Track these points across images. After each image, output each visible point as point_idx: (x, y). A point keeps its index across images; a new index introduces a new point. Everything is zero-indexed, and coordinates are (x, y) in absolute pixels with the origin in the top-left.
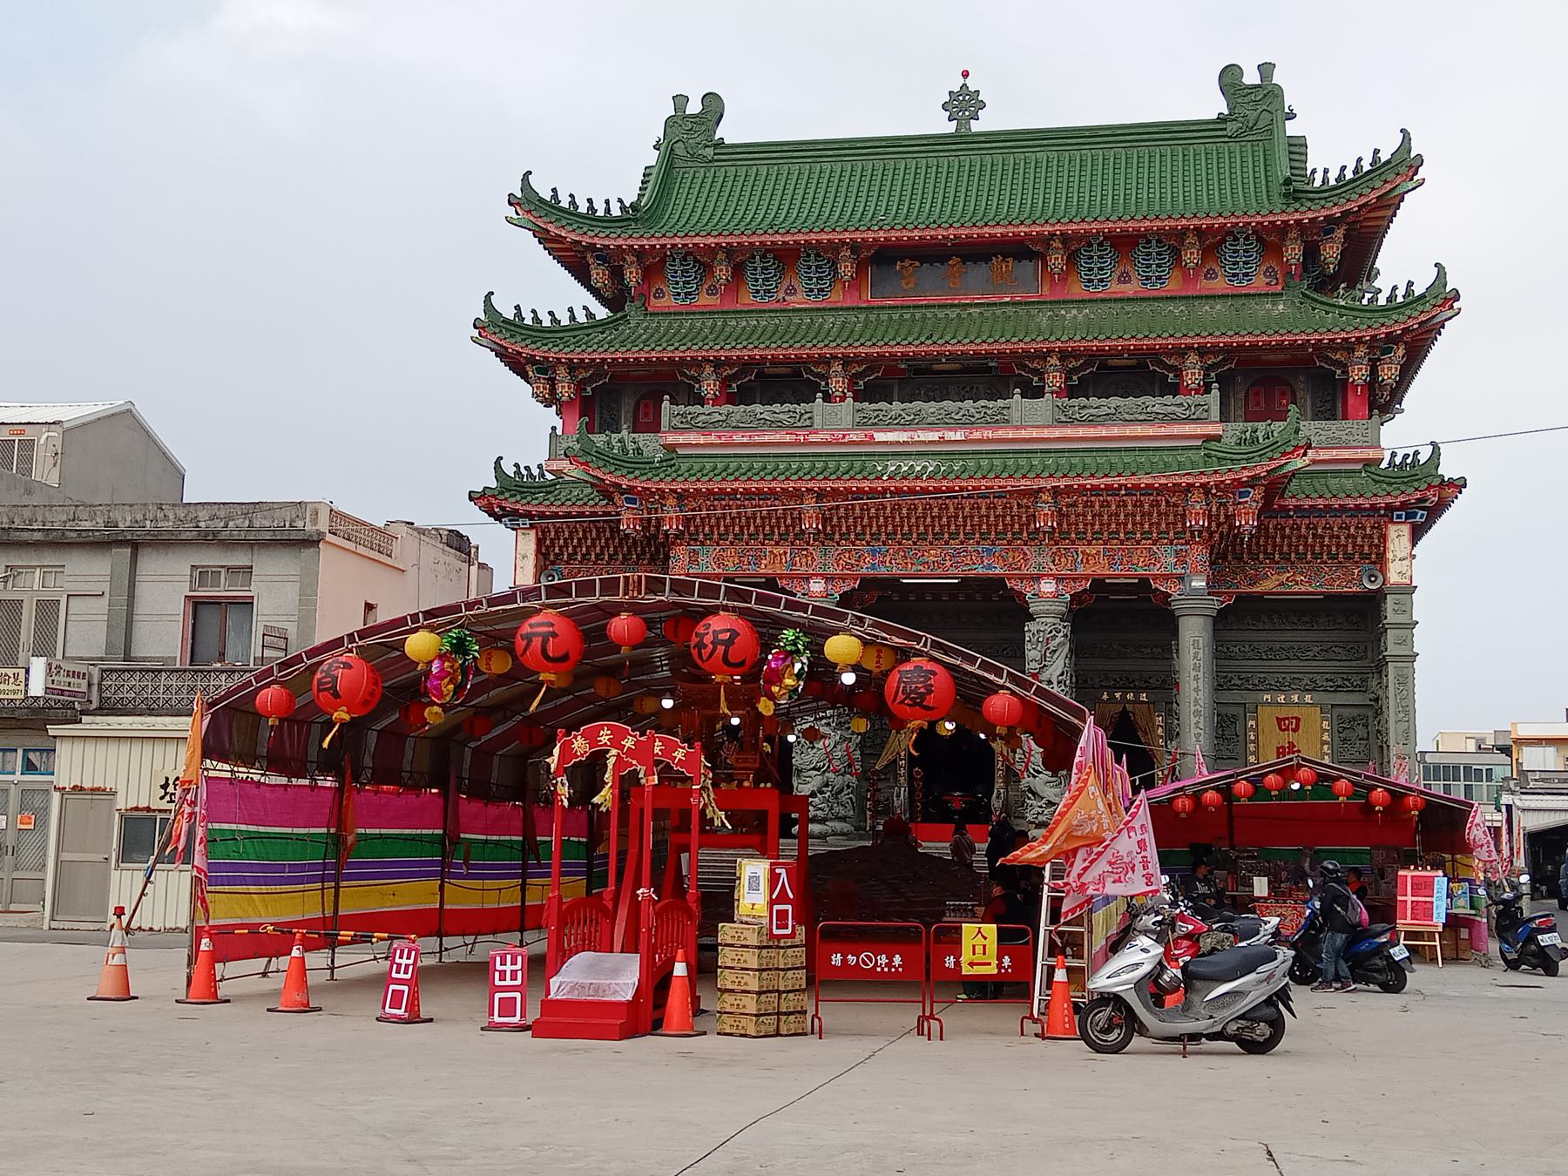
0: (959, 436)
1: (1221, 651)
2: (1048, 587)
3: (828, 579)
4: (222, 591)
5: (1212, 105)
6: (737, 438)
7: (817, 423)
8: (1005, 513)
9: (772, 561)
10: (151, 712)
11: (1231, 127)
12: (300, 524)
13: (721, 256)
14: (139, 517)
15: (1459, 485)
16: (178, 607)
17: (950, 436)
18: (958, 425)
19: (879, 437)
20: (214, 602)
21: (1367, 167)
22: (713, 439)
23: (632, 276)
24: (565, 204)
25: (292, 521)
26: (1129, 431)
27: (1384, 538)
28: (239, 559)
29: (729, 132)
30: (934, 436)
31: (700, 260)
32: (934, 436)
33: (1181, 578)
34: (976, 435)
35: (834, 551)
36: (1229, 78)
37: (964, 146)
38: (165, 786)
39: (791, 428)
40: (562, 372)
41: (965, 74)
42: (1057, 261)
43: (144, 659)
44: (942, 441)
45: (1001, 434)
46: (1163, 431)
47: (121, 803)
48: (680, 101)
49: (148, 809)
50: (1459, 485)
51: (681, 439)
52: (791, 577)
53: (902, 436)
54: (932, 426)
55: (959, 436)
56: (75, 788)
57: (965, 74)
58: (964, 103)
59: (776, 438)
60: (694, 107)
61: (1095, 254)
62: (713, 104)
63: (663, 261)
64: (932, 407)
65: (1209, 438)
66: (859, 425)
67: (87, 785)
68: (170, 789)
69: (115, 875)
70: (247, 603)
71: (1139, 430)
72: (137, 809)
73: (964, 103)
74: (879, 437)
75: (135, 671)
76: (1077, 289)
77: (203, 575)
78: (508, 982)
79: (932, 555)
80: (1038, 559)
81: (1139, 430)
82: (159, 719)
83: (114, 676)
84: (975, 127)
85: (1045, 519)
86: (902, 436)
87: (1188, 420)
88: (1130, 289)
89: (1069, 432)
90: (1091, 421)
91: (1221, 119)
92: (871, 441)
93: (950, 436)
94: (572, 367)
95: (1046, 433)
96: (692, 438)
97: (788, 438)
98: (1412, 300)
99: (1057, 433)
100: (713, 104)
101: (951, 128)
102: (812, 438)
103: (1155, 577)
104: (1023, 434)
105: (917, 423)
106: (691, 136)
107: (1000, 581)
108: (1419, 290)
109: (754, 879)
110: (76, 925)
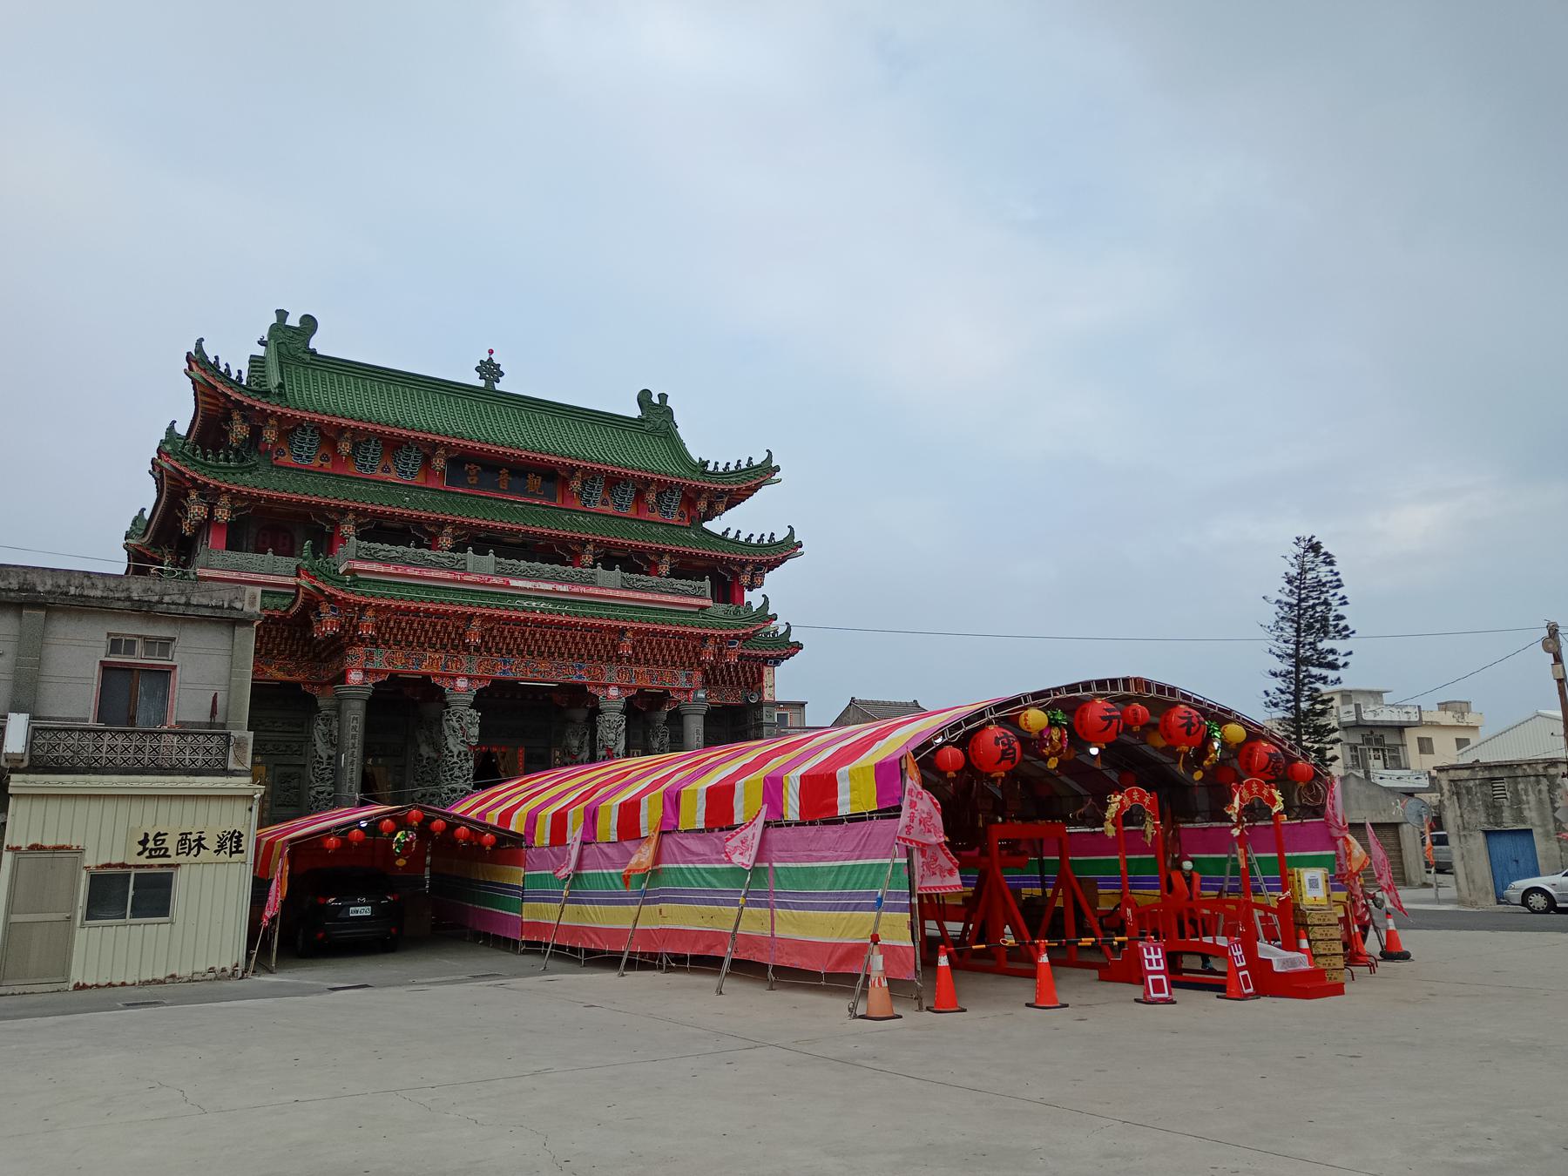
0: (565, 588)
1: (370, 727)
2: (613, 692)
3: (470, 678)
4: (139, 657)
5: (634, 412)
6: (410, 571)
7: (470, 567)
8: (600, 642)
9: (429, 664)
10: (96, 771)
11: (647, 426)
12: (238, 605)
13: (348, 435)
14: (62, 582)
15: (798, 647)
16: (96, 671)
17: (560, 588)
18: (564, 582)
19: (513, 583)
20: (128, 669)
21: (744, 466)
22: (391, 569)
23: (270, 435)
24: (222, 369)
25: (231, 601)
26: (664, 598)
27: (761, 675)
28: (161, 631)
29: (321, 344)
30: (549, 587)
31: (329, 435)
32: (549, 587)
33: (687, 691)
34: (576, 590)
35: (476, 659)
36: (644, 398)
37: (487, 394)
38: (144, 843)
39: (452, 569)
40: (224, 500)
41: (491, 352)
42: (576, 485)
43: (49, 719)
44: (554, 591)
45: (590, 590)
46: (682, 601)
47: (91, 860)
48: (282, 314)
49: (123, 865)
50: (798, 647)
51: (366, 567)
52: (442, 676)
53: (529, 585)
54: (547, 580)
55: (565, 588)
56: (33, 847)
57: (491, 352)
58: (490, 370)
59: (440, 574)
60: (293, 321)
61: (372, 447)
62: (309, 324)
63: (294, 430)
64: (547, 567)
65: (703, 608)
66: (497, 574)
67: (47, 843)
68: (151, 845)
69: (80, 935)
70: (165, 674)
71: (670, 598)
72: (109, 865)
73: (490, 370)
74: (513, 583)
75: (73, 730)
76: (353, 470)
77: (115, 645)
78: (1155, 968)
79: (544, 666)
80: (611, 673)
81: (670, 598)
82: (106, 778)
83: (76, 735)
84: (498, 387)
85: (626, 650)
86: (529, 585)
87: (695, 596)
88: (610, 509)
89: (631, 594)
90: (643, 590)
91: (640, 419)
92: (508, 586)
93: (560, 588)
94: (235, 497)
95: (617, 593)
96: (375, 567)
97: (449, 576)
98: (773, 544)
99: (624, 594)
100: (309, 324)
101: (482, 383)
102: (466, 578)
103: (435, 675)
104: (604, 592)
105: (539, 577)
106: (290, 340)
107: (583, 686)
108: (778, 538)
109: (1314, 884)
110: (28, 989)
